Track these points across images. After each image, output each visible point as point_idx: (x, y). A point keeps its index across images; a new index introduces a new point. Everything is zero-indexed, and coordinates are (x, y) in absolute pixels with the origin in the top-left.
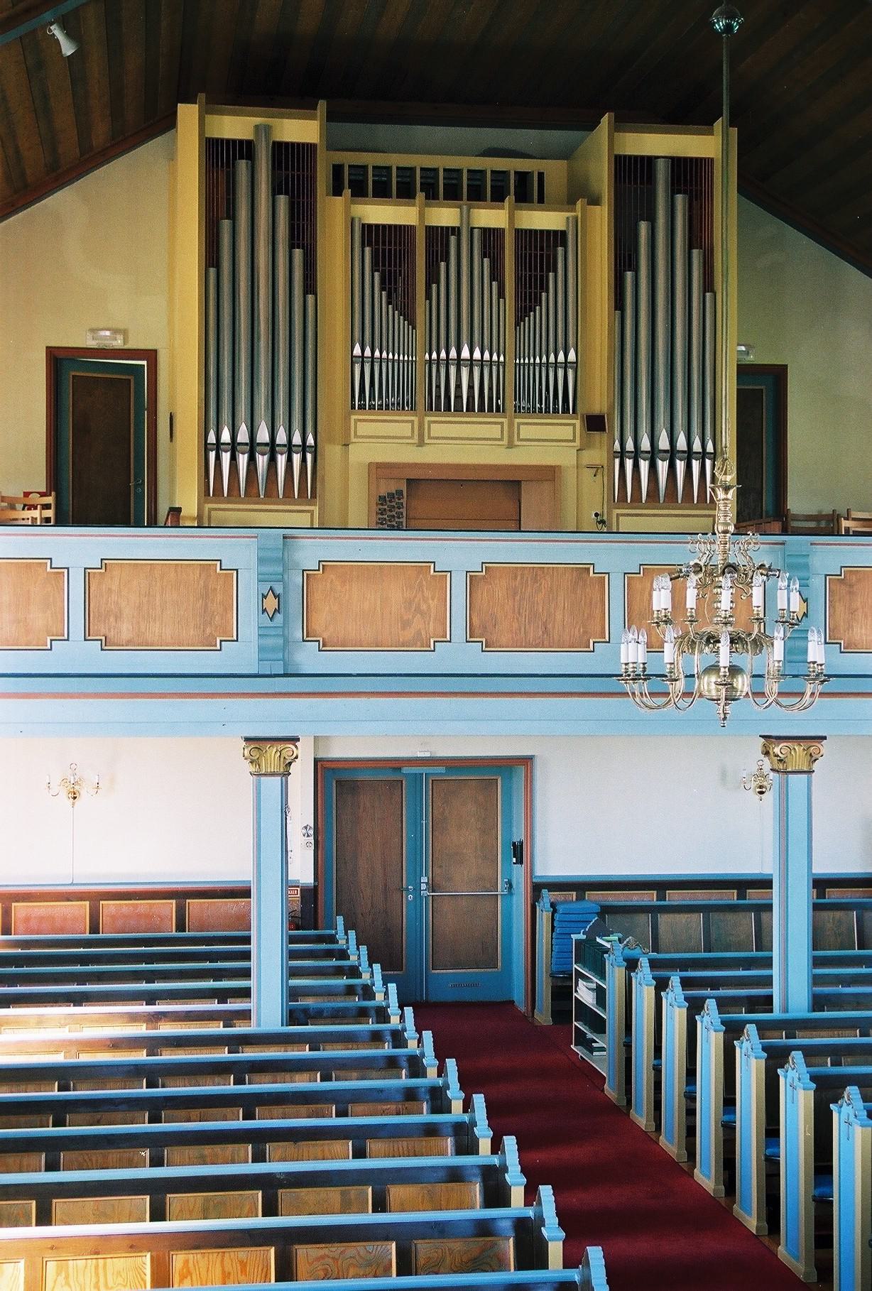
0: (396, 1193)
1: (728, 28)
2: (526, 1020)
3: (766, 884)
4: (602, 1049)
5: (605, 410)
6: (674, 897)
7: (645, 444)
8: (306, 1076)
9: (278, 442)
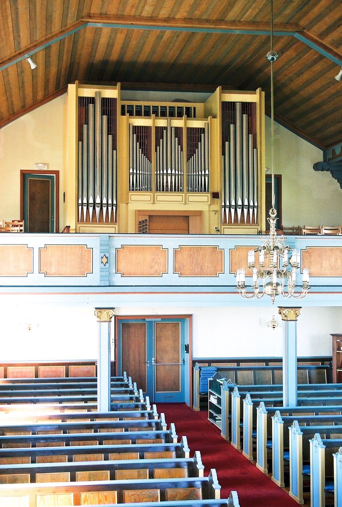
0: (157, 471)
1: (273, 59)
2: (190, 409)
3: (280, 360)
4: (220, 420)
5: (219, 191)
6: (243, 365)
7: (233, 203)
8: (119, 429)
9: (90, 202)
